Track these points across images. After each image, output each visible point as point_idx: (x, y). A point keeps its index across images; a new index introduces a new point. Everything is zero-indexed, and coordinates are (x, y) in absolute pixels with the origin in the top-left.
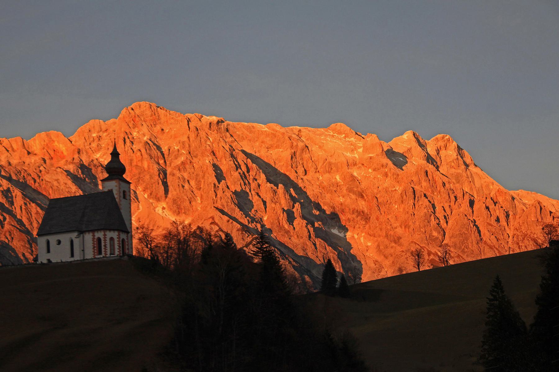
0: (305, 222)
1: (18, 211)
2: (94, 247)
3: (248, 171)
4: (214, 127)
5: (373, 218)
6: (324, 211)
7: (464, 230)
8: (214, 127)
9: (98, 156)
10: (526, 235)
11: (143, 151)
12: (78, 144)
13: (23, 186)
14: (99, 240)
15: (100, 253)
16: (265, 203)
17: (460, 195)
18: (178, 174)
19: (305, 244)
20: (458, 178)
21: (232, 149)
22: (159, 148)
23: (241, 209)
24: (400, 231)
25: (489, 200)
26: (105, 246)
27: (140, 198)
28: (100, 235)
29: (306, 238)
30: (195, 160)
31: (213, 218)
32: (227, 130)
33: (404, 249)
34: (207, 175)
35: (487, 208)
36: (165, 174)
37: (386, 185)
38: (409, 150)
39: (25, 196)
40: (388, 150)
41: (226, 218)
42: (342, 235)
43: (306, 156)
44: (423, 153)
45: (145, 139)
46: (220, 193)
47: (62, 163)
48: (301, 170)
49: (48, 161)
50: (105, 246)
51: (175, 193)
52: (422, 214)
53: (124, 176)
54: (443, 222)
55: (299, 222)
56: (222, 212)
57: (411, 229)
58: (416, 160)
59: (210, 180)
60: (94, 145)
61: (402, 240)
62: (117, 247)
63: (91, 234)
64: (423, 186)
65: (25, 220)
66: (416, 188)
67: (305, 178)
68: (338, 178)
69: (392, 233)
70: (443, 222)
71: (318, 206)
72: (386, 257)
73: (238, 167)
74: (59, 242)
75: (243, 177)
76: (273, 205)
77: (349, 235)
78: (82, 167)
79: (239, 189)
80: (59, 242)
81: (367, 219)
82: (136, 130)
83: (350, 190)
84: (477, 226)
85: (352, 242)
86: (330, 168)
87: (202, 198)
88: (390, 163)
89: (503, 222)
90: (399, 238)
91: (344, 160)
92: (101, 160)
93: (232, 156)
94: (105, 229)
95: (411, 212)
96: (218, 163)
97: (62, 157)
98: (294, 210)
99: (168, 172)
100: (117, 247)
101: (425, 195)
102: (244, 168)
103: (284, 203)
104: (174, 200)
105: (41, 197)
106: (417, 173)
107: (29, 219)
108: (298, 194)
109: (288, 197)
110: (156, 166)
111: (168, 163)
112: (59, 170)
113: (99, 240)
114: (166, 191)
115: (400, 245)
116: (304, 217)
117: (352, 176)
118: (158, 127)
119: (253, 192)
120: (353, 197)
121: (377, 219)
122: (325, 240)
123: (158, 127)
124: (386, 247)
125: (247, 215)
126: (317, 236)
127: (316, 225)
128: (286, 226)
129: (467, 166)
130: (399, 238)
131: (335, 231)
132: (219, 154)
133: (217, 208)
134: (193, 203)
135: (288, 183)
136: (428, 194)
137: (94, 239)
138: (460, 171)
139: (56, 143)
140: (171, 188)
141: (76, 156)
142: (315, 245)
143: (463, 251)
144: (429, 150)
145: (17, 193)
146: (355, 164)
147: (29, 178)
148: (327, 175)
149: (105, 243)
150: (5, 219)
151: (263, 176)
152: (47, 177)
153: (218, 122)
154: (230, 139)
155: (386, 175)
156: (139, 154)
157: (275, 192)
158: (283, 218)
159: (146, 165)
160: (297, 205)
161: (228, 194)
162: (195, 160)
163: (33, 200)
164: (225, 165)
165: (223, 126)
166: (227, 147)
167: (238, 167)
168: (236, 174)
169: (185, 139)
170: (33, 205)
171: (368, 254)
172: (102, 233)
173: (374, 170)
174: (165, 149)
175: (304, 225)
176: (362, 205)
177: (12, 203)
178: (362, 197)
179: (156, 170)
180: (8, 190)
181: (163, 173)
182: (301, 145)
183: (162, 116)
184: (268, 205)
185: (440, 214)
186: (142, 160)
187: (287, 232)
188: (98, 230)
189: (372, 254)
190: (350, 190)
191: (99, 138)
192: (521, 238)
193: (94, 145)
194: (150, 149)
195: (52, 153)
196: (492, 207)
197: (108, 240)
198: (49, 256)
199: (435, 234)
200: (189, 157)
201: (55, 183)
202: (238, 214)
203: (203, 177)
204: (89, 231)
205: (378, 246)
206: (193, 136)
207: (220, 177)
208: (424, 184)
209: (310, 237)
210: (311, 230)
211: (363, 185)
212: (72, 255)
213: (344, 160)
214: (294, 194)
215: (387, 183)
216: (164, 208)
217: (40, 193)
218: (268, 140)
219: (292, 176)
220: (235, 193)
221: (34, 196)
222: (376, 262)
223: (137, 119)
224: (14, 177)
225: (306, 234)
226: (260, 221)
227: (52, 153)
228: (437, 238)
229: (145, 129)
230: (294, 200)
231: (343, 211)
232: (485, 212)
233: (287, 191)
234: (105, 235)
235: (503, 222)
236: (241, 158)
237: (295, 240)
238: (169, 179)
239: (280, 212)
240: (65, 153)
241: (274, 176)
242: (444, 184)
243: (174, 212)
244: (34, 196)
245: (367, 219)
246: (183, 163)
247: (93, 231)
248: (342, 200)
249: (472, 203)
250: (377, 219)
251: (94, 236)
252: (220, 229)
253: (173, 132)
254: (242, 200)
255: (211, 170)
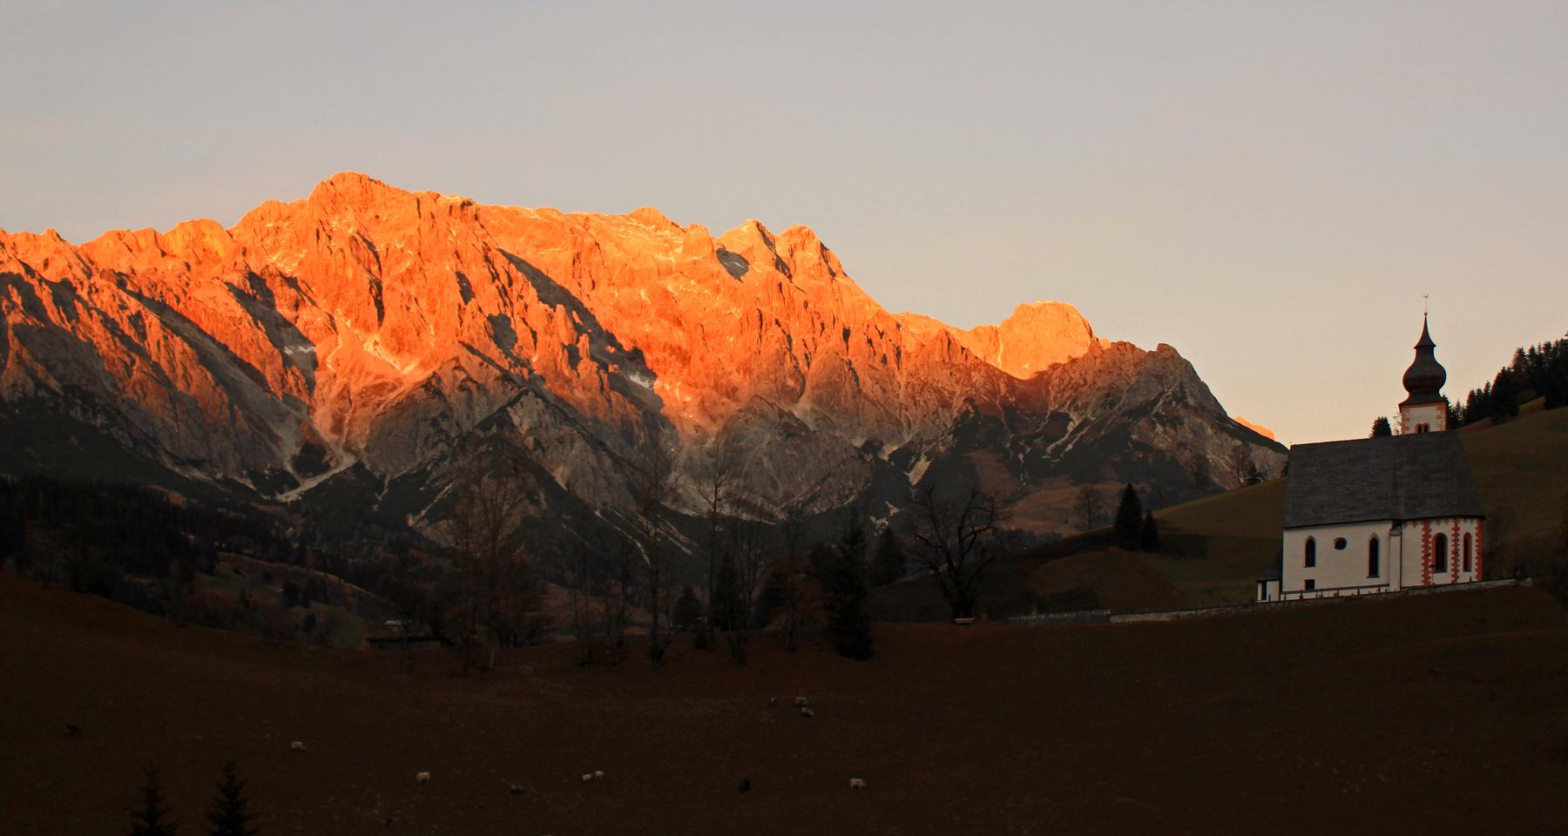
0: (595, 365)
1: (153, 349)
2: (1426, 556)
3: (510, 284)
4: (456, 212)
5: (695, 359)
6: (619, 347)
7: (835, 377)
8: (456, 212)
9: (275, 258)
10: (925, 384)
11: (347, 251)
12: (242, 239)
13: (161, 308)
14: (1441, 539)
15: (1440, 566)
16: (534, 334)
17: (828, 322)
18: (401, 288)
19: (593, 400)
20: (819, 293)
21: (487, 249)
22: (371, 246)
23: (499, 344)
24: (736, 378)
25: (872, 328)
26: (1456, 553)
27: (339, 326)
28: (1446, 528)
29: (596, 390)
30: (427, 266)
31: (457, 359)
32: (476, 218)
33: (742, 406)
34: (446, 291)
35: (870, 341)
36: (380, 289)
37: (717, 305)
38: (750, 249)
39: (164, 325)
40: (718, 252)
41: (478, 360)
42: (646, 385)
43: (596, 259)
44: (771, 255)
45: (351, 231)
46: (467, 319)
47: (216, 270)
48: (587, 282)
49: (193, 267)
50: (1456, 553)
51: (394, 319)
52: (772, 351)
53: (1442, 392)
54: (802, 364)
55: (586, 367)
56: (470, 348)
57: (754, 376)
58: (761, 268)
59: (452, 299)
60: (268, 241)
61: (738, 393)
62: (1474, 554)
63: (1420, 526)
64: (773, 309)
65: (163, 363)
66: (764, 310)
67: (593, 293)
68: (643, 293)
69: (724, 381)
70: (802, 364)
71: (611, 339)
72: (713, 419)
73: (495, 277)
74: (1341, 544)
75: (503, 292)
76: (548, 338)
77: (657, 384)
78: (252, 276)
79: (495, 313)
80: (1341, 544)
81: (685, 359)
82: (337, 217)
83: (661, 314)
84: (854, 372)
85: (662, 395)
86: (631, 279)
87: (437, 326)
88: (724, 270)
89: (892, 364)
90: (735, 389)
91: (653, 264)
92: (279, 265)
93: (487, 259)
94: (1456, 518)
95: (754, 348)
96: (464, 271)
97: (218, 261)
98: (580, 345)
99: (384, 285)
100: (1474, 554)
101: (777, 322)
102: (504, 279)
103: (564, 333)
104: (393, 331)
105: (187, 325)
106: (765, 286)
107: (171, 362)
108: (584, 320)
109: (570, 325)
110: (366, 277)
111: (384, 270)
112: (216, 282)
113: (1441, 539)
114: (381, 316)
115: (736, 400)
116: (593, 358)
117: (665, 291)
118: (371, 213)
119: (517, 318)
120: (666, 324)
121: (702, 359)
122: (624, 393)
123: (371, 213)
124: (715, 404)
125: (508, 354)
126: (613, 388)
127: (611, 369)
128: (567, 372)
129: (833, 275)
130: (735, 389)
131: (635, 379)
132: (468, 255)
133: (463, 344)
134: (423, 335)
135: (573, 304)
136: (781, 320)
137: (1426, 536)
138: (822, 283)
139: (208, 238)
140: (388, 312)
141: (240, 259)
142: (609, 401)
143: (832, 410)
144: (778, 249)
145: (152, 320)
146: (670, 272)
147: (170, 295)
148: (626, 290)
149: (1456, 545)
150: (133, 362)
151: (533, 292)
152: (198, 294)
153: (463, 205)
154: (481, 232)
155: (717, 290)
156: (340, 256)
157: (551, 317)
158: (563, 358)
159: (350, 273)
160: (584, 338)
161: (481, 321)
162: (427, 266)
163: (176, 331)
164: (477, 273)
165: (470, 211)
166: (480, 245)
167: (495, 277)
168: (493, 289)
169: (412, 231)
170: (178, 339)
171: (685, 415)
172: (1451, 524)
173: (699, 282)
174: (380, 248)
175: (595, 369)
176: (679, 337)
177: (144, 336)
178: (679, 324)
179: (366, 282)
180: (139, 315)
181: (377, 287)
182: (588, 241)
183: (378, 196)
184: (539, 337)
185: (798, 351)
186: (345, 265)
187: (568, 381)
188: (1438, 519)
189: (692, 415)
190: (661, 314)
191: (278, 230)
192: (918, 388)
193: (268, 241)
194: (358, 248)
195: (200, 253)
196: (876, 339)
197: (1461, 538)
198: (1310, 573)
199: (790, 383)
200: (418, 259)
201: (211, 304)
202: (494, 351)
203: (441, 293)
204: (1415, 521)
205: (702, 402)
206: (425, 228)
207: (467, 293)
208: (776, 304)
209: (602, 388)
210: (605, 377)
211: (682, 306)
212: (1373, 571)
213: (653, 264)
214: (578, 320)
215: (718, 302)
216: (376, 343)
217: (184, 319)
218: (538, 233)
219: (574, 291)
220: (490, 318)
221: (177, 323)
222: (697, 428)
223: (339, 199)
224: (146, 294)
225: (597, 384)
226: (526, 363)
227: (200, 253)
228: (793, 389)
229: (350, 216)
230: (579, 330)
231: (649, 348)
232: (866, 347)
233: (569, 313)
234: (1456, 529)
235: (892, 364)
236: (500, 263)
237: (579, 394)
238: (387, 297)
239: (558, 349)
240: (222, 254)
241: (551, 293)
242: (806, 304)
243: (392, 350)
244: (177, 323)
245: (685, 359)
246: (409, 271)
247: (1426, 520)
248: (647, 329)
249: (846, 334)
250: (702, 359)
251: (1427, 530)
252: (469, 378)
253: (394, 221)
254: (500, 329)
255: (454, 281)
